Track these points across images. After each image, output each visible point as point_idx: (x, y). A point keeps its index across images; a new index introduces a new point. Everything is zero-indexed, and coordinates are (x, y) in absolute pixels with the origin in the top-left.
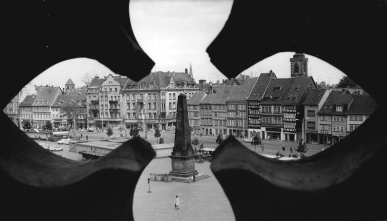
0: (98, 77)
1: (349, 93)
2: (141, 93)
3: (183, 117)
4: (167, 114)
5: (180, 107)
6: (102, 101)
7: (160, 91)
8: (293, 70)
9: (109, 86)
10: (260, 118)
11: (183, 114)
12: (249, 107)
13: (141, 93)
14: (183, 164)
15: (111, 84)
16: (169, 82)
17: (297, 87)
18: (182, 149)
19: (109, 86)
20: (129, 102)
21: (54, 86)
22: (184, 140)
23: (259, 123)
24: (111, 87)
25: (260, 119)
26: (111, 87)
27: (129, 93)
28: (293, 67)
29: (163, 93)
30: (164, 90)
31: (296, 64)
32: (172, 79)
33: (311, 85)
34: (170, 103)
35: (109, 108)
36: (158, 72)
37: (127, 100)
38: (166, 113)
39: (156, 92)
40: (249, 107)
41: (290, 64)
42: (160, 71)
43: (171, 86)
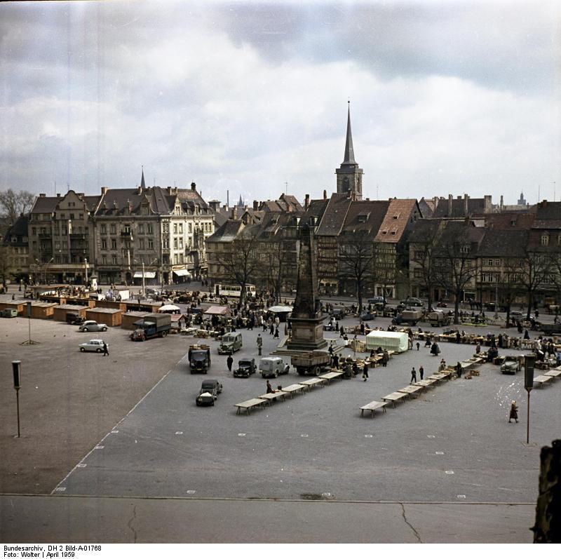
0: (44, 195)
1: (474, 226)
2: (127, 222)
3: (310, 259)
4: (172, 257)
5: (305, 245)
6: (55, 235)
7: (160, 219)
8: (341, 187)
9: (70, 210)
10: (336, 262)
11: (310, 255)
12: (319, 245)
13: (127, 222)
14: (312, 330)
15: (72, 207)
16: (174, 206)
17: (394, 216)
18: (309, 308)
19: (70, 210)
20: (105, 236)
21: (425, 198)
22: (312, 295)
23: (335, 270)
24: (72, 212)
25: (336, 265)
26: (72, 212)
27: (105, 222)
28: (341, 183)
29: (165, 222)
30: (166, 218)
31: (346, 178)
32: (177, 200)
33: (415, 212)
34: (175, 239)
35: (70, 247)
36: (154, 188)
37: (101, 234)
38: (169, 255)
39: (152, 222)
40: (319, 245)
41: (336, 178)
42: (156, 186)
43: (176, 212)
